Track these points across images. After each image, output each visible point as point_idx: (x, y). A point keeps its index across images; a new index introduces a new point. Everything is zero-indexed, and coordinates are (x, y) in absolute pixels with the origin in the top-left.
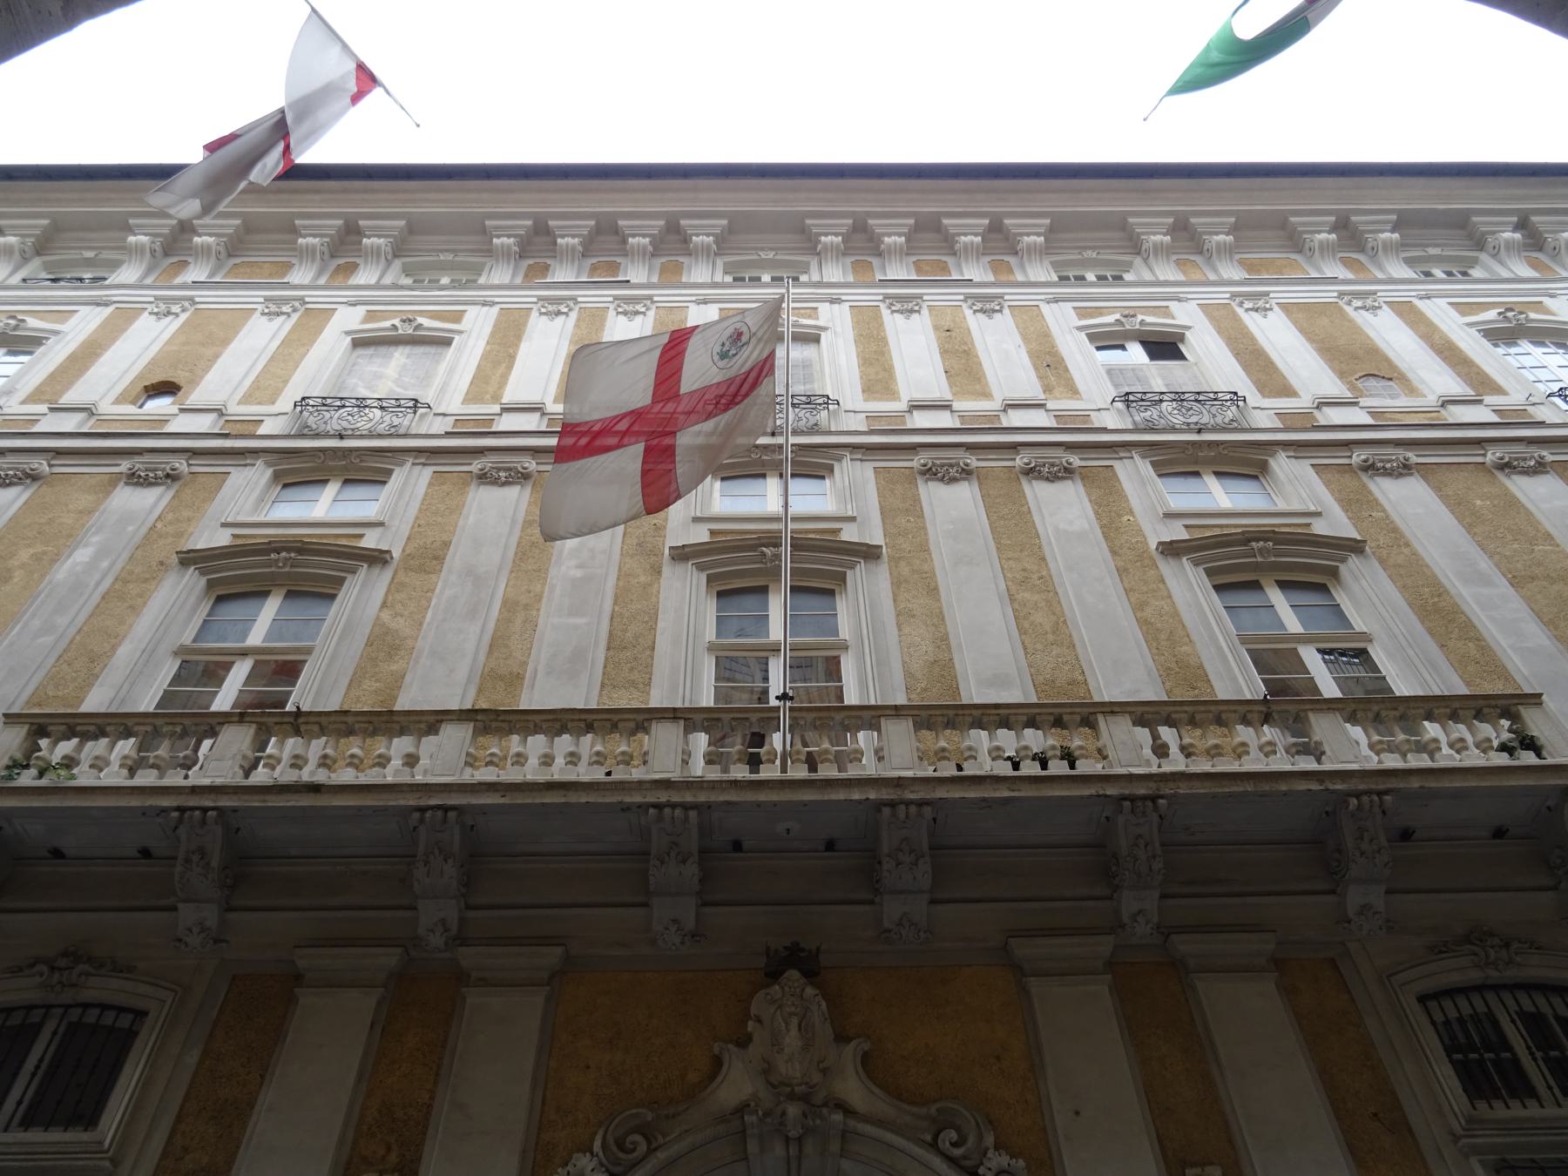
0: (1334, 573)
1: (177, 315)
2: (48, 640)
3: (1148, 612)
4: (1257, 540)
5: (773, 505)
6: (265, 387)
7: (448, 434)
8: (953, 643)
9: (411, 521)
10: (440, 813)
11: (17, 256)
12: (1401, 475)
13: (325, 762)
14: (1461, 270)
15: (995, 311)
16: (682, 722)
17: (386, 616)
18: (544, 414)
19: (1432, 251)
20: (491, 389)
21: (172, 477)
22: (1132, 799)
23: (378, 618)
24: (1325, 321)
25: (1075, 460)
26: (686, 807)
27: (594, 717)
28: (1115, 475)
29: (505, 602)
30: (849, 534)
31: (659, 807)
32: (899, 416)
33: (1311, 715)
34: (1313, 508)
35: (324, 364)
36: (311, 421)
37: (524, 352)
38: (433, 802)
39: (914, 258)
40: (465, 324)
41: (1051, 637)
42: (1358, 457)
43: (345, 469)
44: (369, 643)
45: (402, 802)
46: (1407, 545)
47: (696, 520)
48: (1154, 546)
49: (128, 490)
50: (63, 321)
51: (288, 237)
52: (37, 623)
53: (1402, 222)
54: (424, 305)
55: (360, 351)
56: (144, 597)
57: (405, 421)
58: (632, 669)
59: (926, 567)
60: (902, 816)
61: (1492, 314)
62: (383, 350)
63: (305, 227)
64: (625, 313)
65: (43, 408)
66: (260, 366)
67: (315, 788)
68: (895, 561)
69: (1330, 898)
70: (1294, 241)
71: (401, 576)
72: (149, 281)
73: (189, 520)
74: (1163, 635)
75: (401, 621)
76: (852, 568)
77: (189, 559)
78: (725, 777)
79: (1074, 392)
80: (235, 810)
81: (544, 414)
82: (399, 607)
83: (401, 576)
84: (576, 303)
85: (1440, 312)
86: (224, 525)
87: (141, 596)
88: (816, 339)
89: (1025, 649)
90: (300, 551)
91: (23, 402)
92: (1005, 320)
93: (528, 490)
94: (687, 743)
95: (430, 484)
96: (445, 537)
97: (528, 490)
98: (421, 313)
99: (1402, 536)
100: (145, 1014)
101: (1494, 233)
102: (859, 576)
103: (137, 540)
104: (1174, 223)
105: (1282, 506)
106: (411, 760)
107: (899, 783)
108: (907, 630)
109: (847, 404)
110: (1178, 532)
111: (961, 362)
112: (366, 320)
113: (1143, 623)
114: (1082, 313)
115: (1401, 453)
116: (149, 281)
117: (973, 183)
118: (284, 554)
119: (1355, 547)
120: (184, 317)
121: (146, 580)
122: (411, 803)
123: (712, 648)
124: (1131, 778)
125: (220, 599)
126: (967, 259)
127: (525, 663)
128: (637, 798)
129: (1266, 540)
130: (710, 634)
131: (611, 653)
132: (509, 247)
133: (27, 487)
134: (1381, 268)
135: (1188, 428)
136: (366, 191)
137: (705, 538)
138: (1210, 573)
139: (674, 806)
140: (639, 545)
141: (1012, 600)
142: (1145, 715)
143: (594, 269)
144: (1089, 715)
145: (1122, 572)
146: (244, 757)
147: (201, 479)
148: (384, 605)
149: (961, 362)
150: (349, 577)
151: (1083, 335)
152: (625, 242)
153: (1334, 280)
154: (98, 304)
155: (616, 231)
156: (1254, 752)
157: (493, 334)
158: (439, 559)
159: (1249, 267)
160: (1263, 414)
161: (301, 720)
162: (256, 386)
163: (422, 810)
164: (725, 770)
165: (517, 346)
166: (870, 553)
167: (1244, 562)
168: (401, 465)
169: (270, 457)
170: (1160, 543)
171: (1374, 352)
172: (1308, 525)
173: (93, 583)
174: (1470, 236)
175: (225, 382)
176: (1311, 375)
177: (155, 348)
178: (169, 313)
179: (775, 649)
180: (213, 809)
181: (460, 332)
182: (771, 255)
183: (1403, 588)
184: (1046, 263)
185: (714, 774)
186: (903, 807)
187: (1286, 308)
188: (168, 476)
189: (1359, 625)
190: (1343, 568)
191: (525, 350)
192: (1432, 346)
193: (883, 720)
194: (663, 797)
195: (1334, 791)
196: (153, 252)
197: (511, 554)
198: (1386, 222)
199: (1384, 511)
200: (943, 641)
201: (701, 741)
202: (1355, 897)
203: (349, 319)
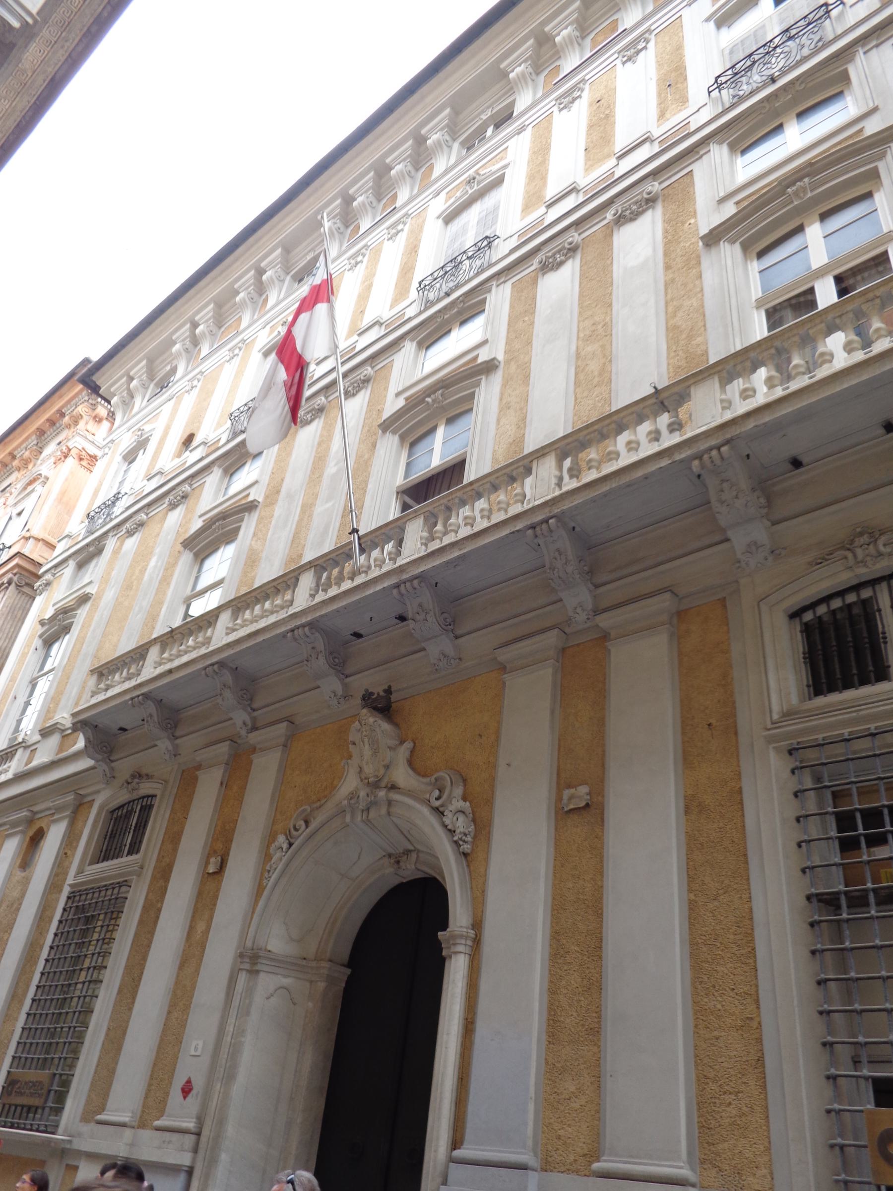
7: (420, 313)
18: (382, 324)
35: (434, 247)
37: (233, 377)
40: (510, 156)
43: (460, 313)
54: (481, 162)
56: (173, 572)
63: (509, 65)
65: (355, 338)
69: (725, 546)
77: (386, 426)
81: (382, 324)
90: (224, 518)
91: (346, 340)
100: (155, 796)
117: (433, 81)
118: (806, 180)
120: (199, 385)
125: (413, 445)
133: (367, 388)
167: (764, 223)
169: (218, 463)
172: (861, 130)
178: (357, 263)
195: (681, 461)
196: (187, 350)
202: (739, 539)
203: (439, 205)
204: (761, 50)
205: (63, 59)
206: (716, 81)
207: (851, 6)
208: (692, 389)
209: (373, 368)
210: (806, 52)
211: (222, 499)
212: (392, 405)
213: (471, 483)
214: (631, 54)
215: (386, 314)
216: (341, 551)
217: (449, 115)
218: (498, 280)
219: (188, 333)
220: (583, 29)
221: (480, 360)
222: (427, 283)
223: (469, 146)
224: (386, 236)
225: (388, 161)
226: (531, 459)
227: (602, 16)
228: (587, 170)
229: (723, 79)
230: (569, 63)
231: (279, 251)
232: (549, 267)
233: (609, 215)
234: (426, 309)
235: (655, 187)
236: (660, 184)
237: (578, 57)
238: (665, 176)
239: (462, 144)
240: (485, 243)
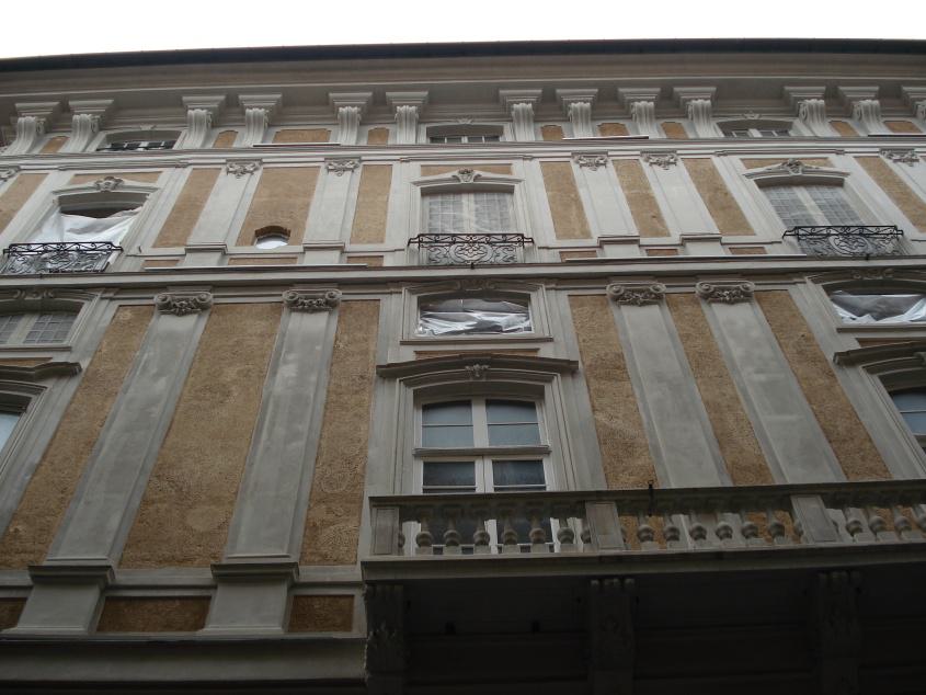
2: (301, 444)
11: (90, 131)
15: (669, 163)
17: (601, 417)
25: (751, 285)
28: (789, 296)
30: (546, 352)
32: (672, 249)
39: (663, 121)
40: (160, 183)
48: (830, 357)
51: (180, 110)
52: (280, 431)
54: (127, 170)
57: (519, 253)
66: (351, 213)
72: (36, 152)
74: (843, 433)
79: (748, 230)
84: (361, 161)
86: (403, 343)
87: (360, 405)
88: (510, 191)
92: (680, 171)
93: (203, 321)
94: (401, 528)
97: (335, 320)
104: (879, 91)
109: (540, 242)
110: (851, 343)
111: (643, 203)
112: (73, 182)
114: (748, 164)
116: (36, 152)
117: (704, 56)
118: (477, 367)
126: (868, 120)
134: (863, 127)
135: (855, 257)
138: (884, 380)
142: (835, 496)
143: (278, 136)
144: (782, 497)
149: (643, 203)
151: (751, 182)
156: (736, 534)
164: (438, 551)
166: (567, 368)
167: (441, 382)
168: (90, 299)
170: (837, 354)
172: (536, 350)
173: (312, 396)
177: (248, 201)
181: (155, 189)
182: (756, 117)
184: (714, 123)
188: (327, 303)
193: (588, 506)
198: (871, 92)
201: (414, 529)
203: (58, 181)
204: (464, 237)
206: (419, 237)
207: (540, 248)
210: (500, 259)
217: (54, 107)
218: (105, 292)
219: (216, 105)
220: (275, 119)
223: (116, 145)
227: (317, 119)
229: (425, 239)
231: (222, 98)
233: (157, 298)
236: (215, 297)
237: (260, 139)
238: (347, 289)
239: (109, 138)
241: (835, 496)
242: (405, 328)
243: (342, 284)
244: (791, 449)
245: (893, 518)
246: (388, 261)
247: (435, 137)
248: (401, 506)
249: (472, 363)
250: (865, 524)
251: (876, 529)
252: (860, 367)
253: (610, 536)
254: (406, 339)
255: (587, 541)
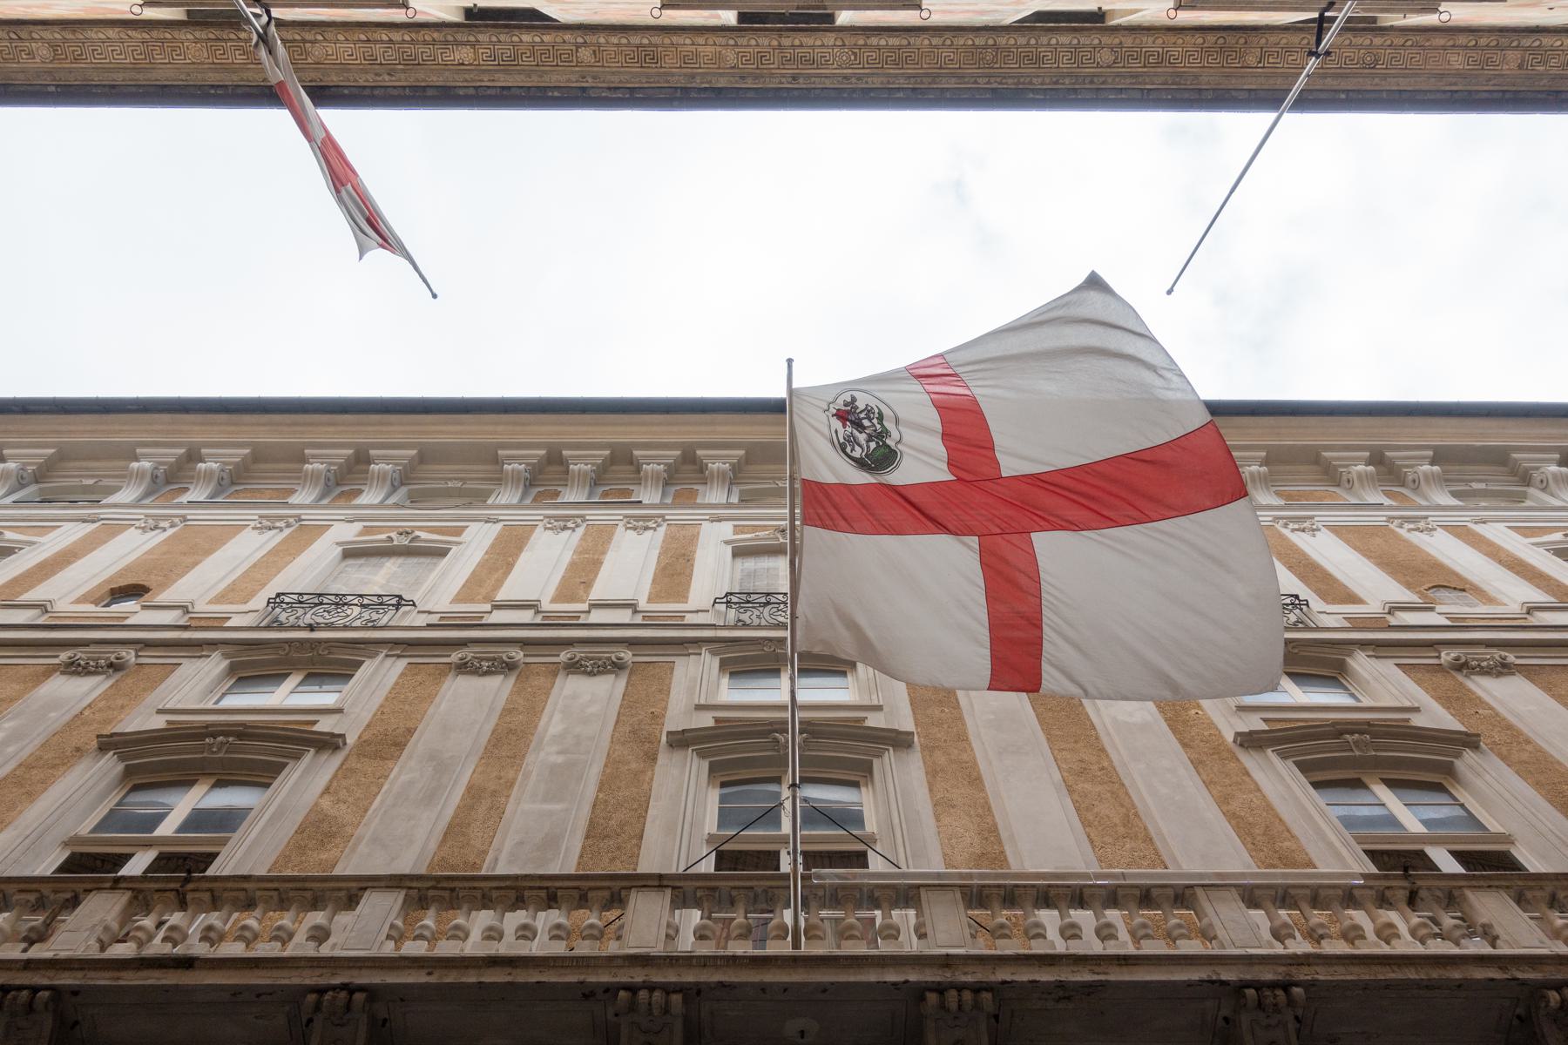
0: (1449, 770)
1: (165, 530)
3: (1235, 806)
4: (1352, 733)
5: (782, 696)
6: (236, 591)
7: (257, 628)
8: (1004, 835)
9: (374, 709)
10: (343, 994)
12: (1499, 675)
13: (208, 935)
14: (1517, 499)
16: (669, 892)
19: (1476, 486)
20: (483, 591)
21: (115, 667)
22: (1258, 986)
23: (316, 804)
24: (1378, 541)
26: (668, 989)
27: (558, 884)
29: (469, 788)
30: (874, 721)
31: (632, 989)
33: (1469, 893)
34: (1408, 704)
36: (283, 617)
38: (337, 981)
40: (465, 536)
41: (1121, 830)
42: (1447, 656)
43: (312, 662)
44: (300, 830)
45: (296, 981)
46: (1528, 741)
47: (699, 707)
48: (1229, 737)
49: (64, 678)
50: (41, 535)
53: (1440, 456)
54: (424, 524)
55: (351, 562)
56: (46, 783)
58: (612, 860)
59: (965, 757)
60: (954, 1006)
61: (1558, 536)
62: (374, 560)
63: (314, 456)
64: (635, 529)
66: (239, 572)
67: (188, 963)
68: (928, 750)
70: (1331, 475)
71: (353, 763)
73: (122, 707)
74: (1257, 827)
75: (343, 807)
76: (880, 756)
77: (108, 744)
78: (721, 952)
80: (75, 992)
82: (343, 794)
83: (353, 763)
85: (1498, 533)
89: (1091, 841)
90: (240, 735)
93: (512, 680)
95: (402, 674)
96: (410, 724)
98: (421, 528)
99: (1520, 733)
101: (1411, 466)
102: (888, 764)
103: (57, 726)
105: (1366, 702)
106: (320, 935)
107: (947, 962)
108: (946, 820)
110: (1255, 723)
112: (361, 534)
113: (1231, 816)
115: (1497, 653)
119: (1469, 741)
120: (170, 532)
121: (54, 767)
122: (307, 982)
123: (711, 838)
124: (1250, 960)
125: (136, 788)
127: (485, 852)
128: (605, 978)
129: (1361, 733)
130: (711, 825)
131: (590, 842)
132: (519, 472)
136: (381, 424)
137: (711, 723)
139: (652, 987)
140: (634, 732)
141: (1071, 790)
145: (1197, 764)
146: (106, 929)
147: (147, 670)
148: (327, 791)
150: (292, 763)
152: (638, 471)
153: (1380, 506)
154: (84, 521)
155: (631, 461)
156: (1123, 935)
157: (493, 546)
158: (400, 745)
159: (1288, 496)
160: (1329, 617)
161: (190, 886)
162: (232, 588)
163: (321, 991)
165: (518, 556)
166: (899, 741)
169: (229, 649)
170: (1238, 734)
171: (1437, 567)
172: (1408, 720)
174: (1513, 473)
175: (200, 587)
176: (1377, 590)
178: (156, 527)
179: (784, 840)
180: (46, 988)
183: (1537, 785)
185: (706, 949)
186: (953, 993)
187: (1336, 530)
188: (111, 665)
189: (1494, 826)
190: (1457, 763)
191: (525, 559)
192: (1500, 562)
194: (638, 976)
195: (1523, 983)
196: (154, 478)
197: (484, 740)
198: (1424, 458)
199: (1491, 708)
200: (990, 832)
203: (348, 532)
205: (361, 83)
208: (367, 893)
209: (137, 656)
211: (210, 705)
212: (143, 719)
213: (215, 879)
214: (562, 524)
215: (202, 607)
216: (276, 885)
221: (315, 728)
222: (287, 600)
223: (415, 499)
224: (252, 524)
225: (204, 451)
226: (89, 886)
228: (554, 601)
230: (571, 495)
231: (414, 452)
232: (74, 669)
234: (268, 628)
235: (627, 655)
238: (634, 652)
240: (394, 601)
241: (1251, 896)
242: (700, 689)
243: (632, 643)
244: (1195, 836)
245: (1166, 920)
246: (690, 619)
247: (745, 501)
248: (674, 888)
249: (214, 735)
250: (1403, 928)
251: (844, 934)
252: (1269, 751)
253: (948, 932)
254: (702, 702)
255: (922, 936)
